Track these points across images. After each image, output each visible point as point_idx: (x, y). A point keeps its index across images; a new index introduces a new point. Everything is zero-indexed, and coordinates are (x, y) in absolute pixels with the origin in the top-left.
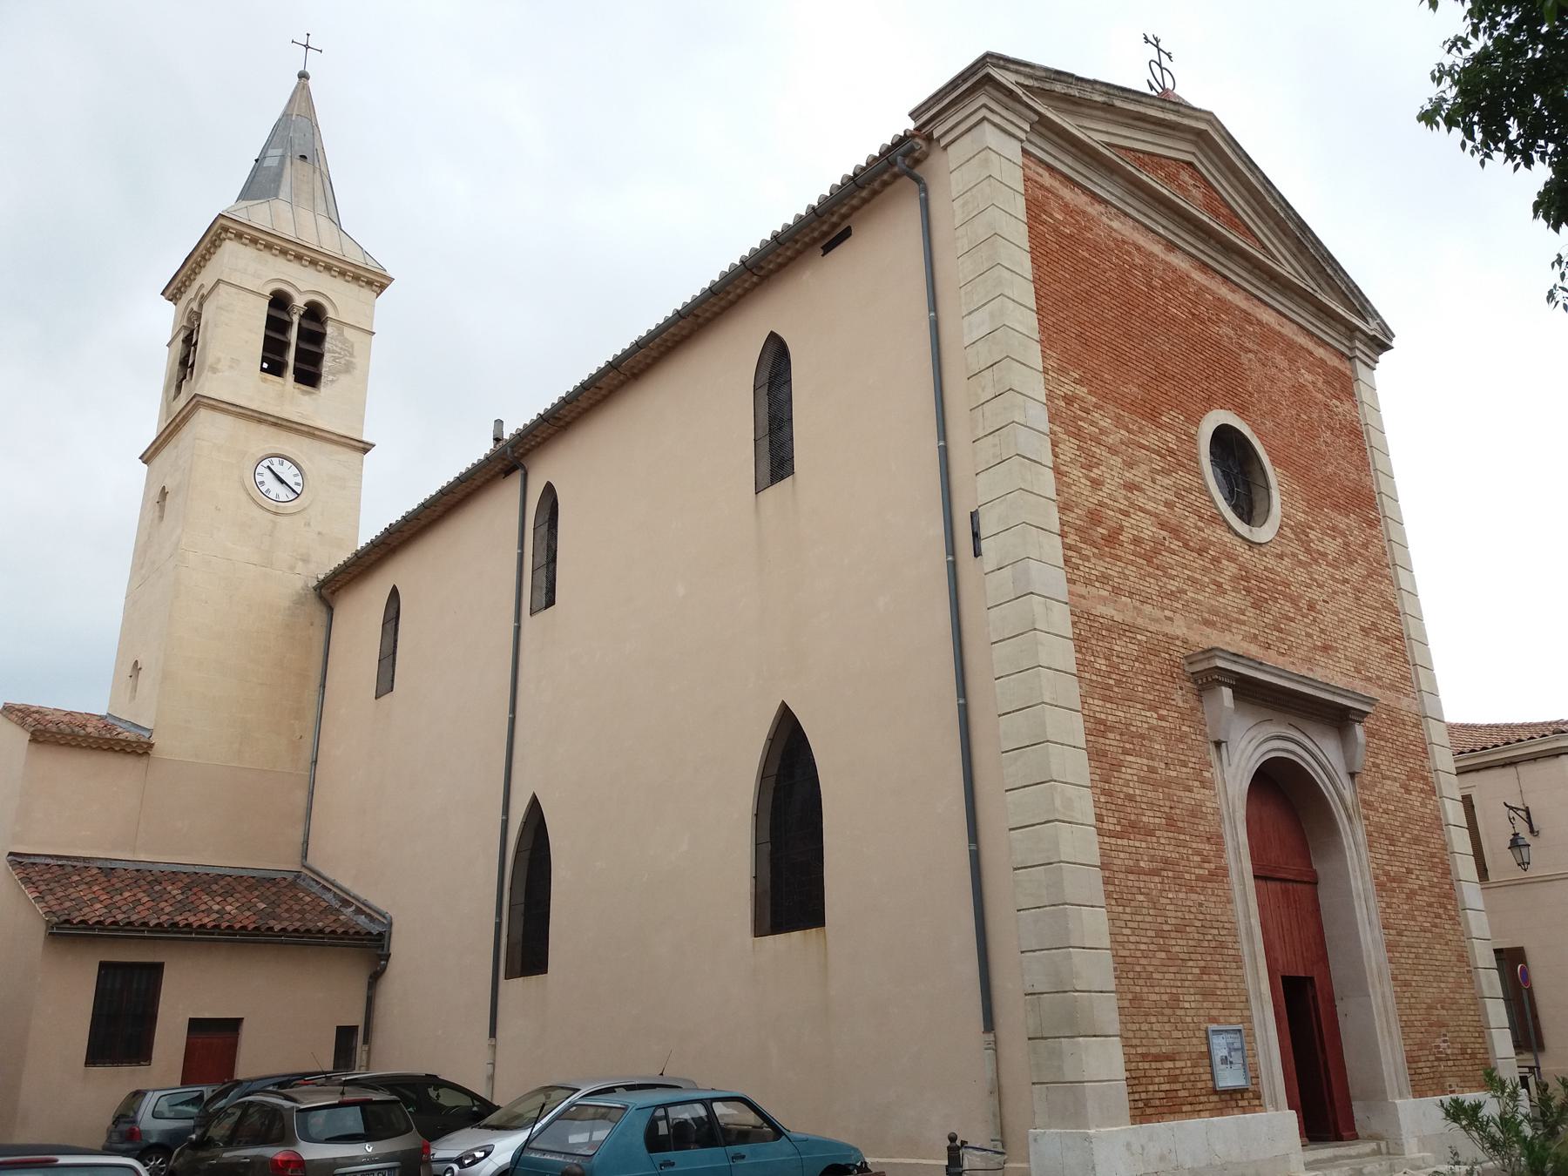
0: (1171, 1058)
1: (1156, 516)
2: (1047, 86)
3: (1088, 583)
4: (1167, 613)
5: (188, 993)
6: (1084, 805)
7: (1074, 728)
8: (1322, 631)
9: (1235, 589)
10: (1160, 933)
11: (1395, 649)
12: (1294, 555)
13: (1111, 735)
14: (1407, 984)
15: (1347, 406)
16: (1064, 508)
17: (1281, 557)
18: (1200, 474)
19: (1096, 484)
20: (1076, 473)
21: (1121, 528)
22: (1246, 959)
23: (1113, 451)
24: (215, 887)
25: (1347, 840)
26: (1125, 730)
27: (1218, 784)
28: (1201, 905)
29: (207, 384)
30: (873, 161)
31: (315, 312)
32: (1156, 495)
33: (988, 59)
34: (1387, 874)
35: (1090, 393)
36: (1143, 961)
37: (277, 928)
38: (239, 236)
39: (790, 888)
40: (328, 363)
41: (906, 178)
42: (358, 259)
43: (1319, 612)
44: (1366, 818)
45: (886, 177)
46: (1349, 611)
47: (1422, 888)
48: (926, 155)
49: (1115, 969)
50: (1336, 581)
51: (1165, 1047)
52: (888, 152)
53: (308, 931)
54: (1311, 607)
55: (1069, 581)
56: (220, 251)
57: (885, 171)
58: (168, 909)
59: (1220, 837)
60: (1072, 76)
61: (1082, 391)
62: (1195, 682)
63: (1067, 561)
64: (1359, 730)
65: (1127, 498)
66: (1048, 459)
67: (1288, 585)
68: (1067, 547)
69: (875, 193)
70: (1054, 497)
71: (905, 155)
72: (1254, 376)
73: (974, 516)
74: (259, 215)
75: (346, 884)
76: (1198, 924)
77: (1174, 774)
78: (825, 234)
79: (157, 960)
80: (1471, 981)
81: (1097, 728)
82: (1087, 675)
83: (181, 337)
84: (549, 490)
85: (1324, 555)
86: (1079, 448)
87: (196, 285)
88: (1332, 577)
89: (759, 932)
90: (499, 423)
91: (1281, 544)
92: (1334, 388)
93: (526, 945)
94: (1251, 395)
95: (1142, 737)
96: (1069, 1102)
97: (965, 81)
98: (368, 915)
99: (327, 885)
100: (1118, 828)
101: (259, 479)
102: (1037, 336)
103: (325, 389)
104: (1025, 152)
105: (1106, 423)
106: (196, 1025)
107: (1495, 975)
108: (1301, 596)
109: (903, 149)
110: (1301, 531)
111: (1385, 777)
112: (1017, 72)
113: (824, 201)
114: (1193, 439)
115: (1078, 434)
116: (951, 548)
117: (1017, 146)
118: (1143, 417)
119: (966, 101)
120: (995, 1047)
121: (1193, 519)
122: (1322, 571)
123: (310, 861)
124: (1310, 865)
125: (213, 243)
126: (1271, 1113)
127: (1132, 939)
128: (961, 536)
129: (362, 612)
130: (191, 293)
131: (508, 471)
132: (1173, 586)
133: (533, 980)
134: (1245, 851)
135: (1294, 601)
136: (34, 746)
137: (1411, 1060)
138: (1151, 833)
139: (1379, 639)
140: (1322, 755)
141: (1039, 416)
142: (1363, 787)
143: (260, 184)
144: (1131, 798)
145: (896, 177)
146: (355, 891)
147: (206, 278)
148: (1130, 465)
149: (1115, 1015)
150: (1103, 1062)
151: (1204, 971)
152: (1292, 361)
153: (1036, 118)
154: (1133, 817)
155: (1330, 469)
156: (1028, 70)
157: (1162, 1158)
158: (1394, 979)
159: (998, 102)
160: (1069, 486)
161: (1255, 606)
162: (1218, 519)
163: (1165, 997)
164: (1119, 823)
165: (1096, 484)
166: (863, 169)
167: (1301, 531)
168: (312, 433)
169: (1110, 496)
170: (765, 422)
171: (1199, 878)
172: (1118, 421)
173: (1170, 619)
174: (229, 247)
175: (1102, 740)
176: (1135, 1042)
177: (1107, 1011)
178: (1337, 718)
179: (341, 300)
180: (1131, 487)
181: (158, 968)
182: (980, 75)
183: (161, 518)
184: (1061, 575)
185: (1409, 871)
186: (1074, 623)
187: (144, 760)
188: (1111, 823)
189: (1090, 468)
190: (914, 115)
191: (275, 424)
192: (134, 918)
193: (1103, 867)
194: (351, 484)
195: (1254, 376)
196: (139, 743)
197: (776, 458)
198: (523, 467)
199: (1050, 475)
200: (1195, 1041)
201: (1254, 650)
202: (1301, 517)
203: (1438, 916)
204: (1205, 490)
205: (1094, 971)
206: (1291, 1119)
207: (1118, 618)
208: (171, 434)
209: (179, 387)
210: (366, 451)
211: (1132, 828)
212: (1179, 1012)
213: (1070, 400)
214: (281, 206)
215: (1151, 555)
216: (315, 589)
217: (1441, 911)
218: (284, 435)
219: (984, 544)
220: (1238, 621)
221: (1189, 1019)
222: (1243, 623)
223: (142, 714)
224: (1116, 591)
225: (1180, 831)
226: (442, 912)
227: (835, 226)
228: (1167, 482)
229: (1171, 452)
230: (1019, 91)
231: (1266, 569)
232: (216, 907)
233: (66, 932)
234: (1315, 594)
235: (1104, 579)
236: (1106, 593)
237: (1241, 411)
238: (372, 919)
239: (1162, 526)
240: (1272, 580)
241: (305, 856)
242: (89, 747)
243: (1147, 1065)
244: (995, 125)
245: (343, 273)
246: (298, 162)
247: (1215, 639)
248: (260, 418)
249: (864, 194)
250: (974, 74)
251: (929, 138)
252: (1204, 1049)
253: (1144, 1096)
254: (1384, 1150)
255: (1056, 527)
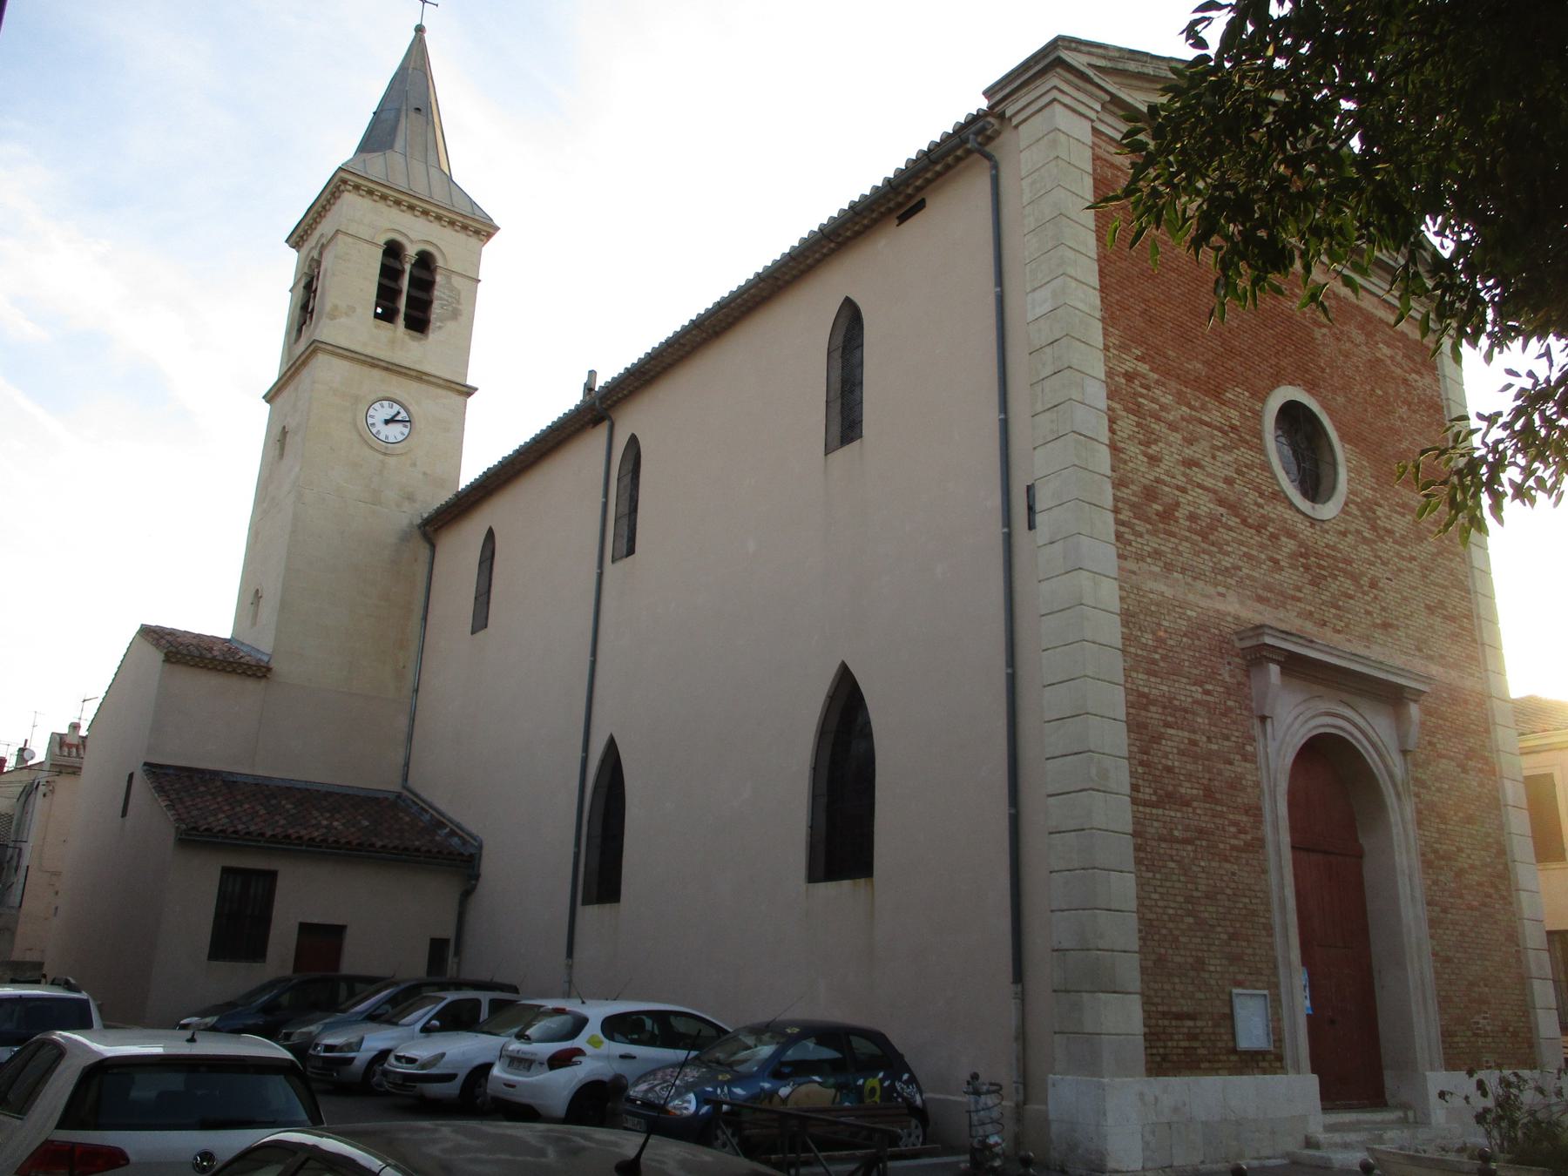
0: (1191, 1017)
1: (1215, 492)
2: (1120, 66)
3: (1140, 558)
4: (1220, 589)
5: (303, 895)
6: (1121, 778)
7: (1116, 701)
8: (1383, 609)
9: (1293, 566)
10: (1189, 899)
11: (1463, 629)
12: (1358, 532)
13: (1153, 709)
14: (1448, 960)
15: (1428, 380)
16: (1119, 484)
17: (1344, 534)
18: (1262, 450)
19: (1154, 460)
20: (1133, 449)
21: (1178, 504)
22: (1278, 929)
23: (1173, 427)
24: (325, 804)
25: (1394, 817)
26: (1168, 705)
27: (1261, 759)
28: (1234, 874)
29: (325, 330)
30: (947, 138)
31: (425, 261)
32: (1216, 471)
33: (1059, 42)
34: (1436, 852)
35: (1152, 370)
36: (1171, 925)
37: (379, 844)
38: (357, 187)
39: (842, 835)
40: (436, 310)
41: (977, 156)
42: (467, 210)
43: (1382, 590)
44: (1417, 795)
45: (959, 153)
46: (1415, 589)
47: (1472, 867)
48: (998, 133)
49: (1140, 931)
50: (1403, 558)
51: (1186, 1006)
52: (961, 129)
53: (406, 849)
54: (1373, 584)
55: (1120, 556)
56: (339, 202)
57: (958, 147)
58: (282, 822)
59: (1260, 809)
60: (1147, 54)
61: (1143, 368)
62: (1244, 658)
63: (1119, 536)
64: (1414, 710)
65: (1184, 475)
66: (1105, 436)
67: (1349, 562)
68: (1118, 522)
69: (948, 168)
70: (1109, 473)
71: (977, 133)
72: (1326, 351)
73: (1030, 490)
74: (376, 167)
75: (442, 807)
76: (1229, 891)
77: (1215, 747)
78: (900, 205)
79: (272, 867)
80: (1519, 960)
81: (1138, 702)
82: (1132, 650)
83: (302, 283)
84: (633, 441)
85: (1390, 532)
86: (1138, 425)
87: (317, 234)
88: (1398, 554)
89: (812, 878)
90: (592, 374)
91: (1345, 521)
92: (1413, 361)
93: (601, 875)
94: (1323, 370)
95: (1186, 711)
96: (1087, 1054)
97: (1037, 63)
98: (460, 837)
99: (423, 807)
100: (1154, 798)
101: (370, 421)
102: (1098, 314)
103: (434, 335)
104: (1095, 131)
105: (1167, 399)
106: (306, 929)
107: (1545, 956)
108: (1363, 574)
109: (974, 128)
110: (1368, 509)
111: (1440, 756)
112: (1089, 53)
113: (900, 173)
114: (1258, 416)
115: (1137, 410)
116: (1007, 521)
117: (1088, 125)
118: (1206, 393)
119: (1038, 82)
120: (1022, 998)
121: (1253, 495)
122: (1387, 548)
123: (411, 782)
124: (1356, 840)
125: (333, 194)
126: (1292, 1076)
127: (1160, 903)
128: (1017, 508)
129: (463, 543)
130: (312, 241)
131: (596, 421)
132: (1227, 562)
133: (607, 908)
134: (1284, 824)
135: (1355, 578)
136: (168, 666)
137: (1447, 1034)
138: (1188, 804)
139: (1445, 617)
140: (1370, 729)
141: (1097, 394)
142: (1416, 765)
143: (378, 137)
144: (1169, 769)
145: (969, 152)
146: (450, 814)
147: (326, 227)
148: (1190, 441)
149: (1136, 974)
150: (1122, 1017)
151: (1233, 936)
152: (1369, 335)
153: (1108, 98)
154: (1170, 788)
155: (1404, 445)
156: (1100, 51)
157: (1176, 1110)
158: (1435, 954)
159: (1067, 82)
160: (1125, 462)
161: (1313, 583)
162: (1278, 496)
163: (1190, 960)
164: (1155, 793)
165: (1154, 460)
166: (938, 145)
167: (1367, 508)
168: (420, 377)
169: (1167, 473)
170: (837, 386)
171: (1233, 848)
172: (1181, 398)
173: (1223, 595)
174: (349, 198)
175: (1143, 713)
176: (1157, 1000)
177: (1129, 970)
178: (1392, 696)
179: (446, 244)
180: (1190, 463)
181: (272, 876)
182: (1051, 58)
183: (281, 455)
184: (1112, 551)
185: (1460, 850)
186: (1122, 599)
187: (263, 682)
188: (1147, 793)
189: (1148, 444)
190: (988, 93)
191: (386, 369)
192: (252, 828)
193: (1135, 834)
194: (453, 430)
195: (1326, 351)
196: (259, 667)
197: (846, 422)
198: (610, 418)
199: (1105, 452)
200: (1218, 1003)
201: (1309, 627)
202: (1368, 493)
203: (1490, 896)
204: (1266, 466)
205: (1121, 933)
206: (1312, 1082)
207: (1169, 593)
208: (292, 377)
209: (300, 331)
210: (469, 394)
211: (1168, 798)
212: (1206, 975)
213: (1130, 377)
214: (396, 158)
215: (1206, 531)
216: (419, 527)
217: (1492, 891)
218: (395, 379)
219: (1039, 518)
220: (1294, 598)
221: (1213, 982)
222: (1299, 600)
223: (263, 643)
224: (1169, 567)
225: (1217, 802)
226: (529, 843)
227: (910, 197)
228: (1227, 458)
229: (1233, 428)
230: (1090, 72)
231: (1327, 546)
232: (325, 822)
233: (192, 838)
234: (1377, 571)
235: (1157, 554)
236: (1157, 569)
237: (1312, 387)
238: (465, 842)
239: (1221, 502)
240: (1333, 557)
241: (405, 779)
242: (215, 669)
243: (1166, 1023)
244: (1066, 106)
245: (452, 223)
246: (413, 115)
247: (1266, 615)
248: (373, 363)
249: (938, 168)
250: (1045, 57)
251: (1001, 116)
252: (1227, 1010)
253: (1161, 1051)
254: (1411, 1119)
255: (1109, 502)
